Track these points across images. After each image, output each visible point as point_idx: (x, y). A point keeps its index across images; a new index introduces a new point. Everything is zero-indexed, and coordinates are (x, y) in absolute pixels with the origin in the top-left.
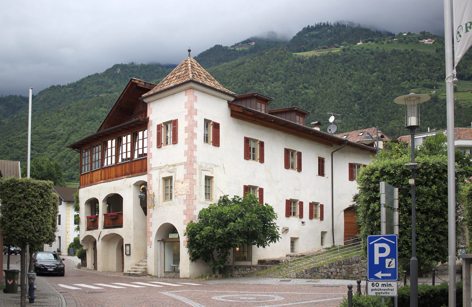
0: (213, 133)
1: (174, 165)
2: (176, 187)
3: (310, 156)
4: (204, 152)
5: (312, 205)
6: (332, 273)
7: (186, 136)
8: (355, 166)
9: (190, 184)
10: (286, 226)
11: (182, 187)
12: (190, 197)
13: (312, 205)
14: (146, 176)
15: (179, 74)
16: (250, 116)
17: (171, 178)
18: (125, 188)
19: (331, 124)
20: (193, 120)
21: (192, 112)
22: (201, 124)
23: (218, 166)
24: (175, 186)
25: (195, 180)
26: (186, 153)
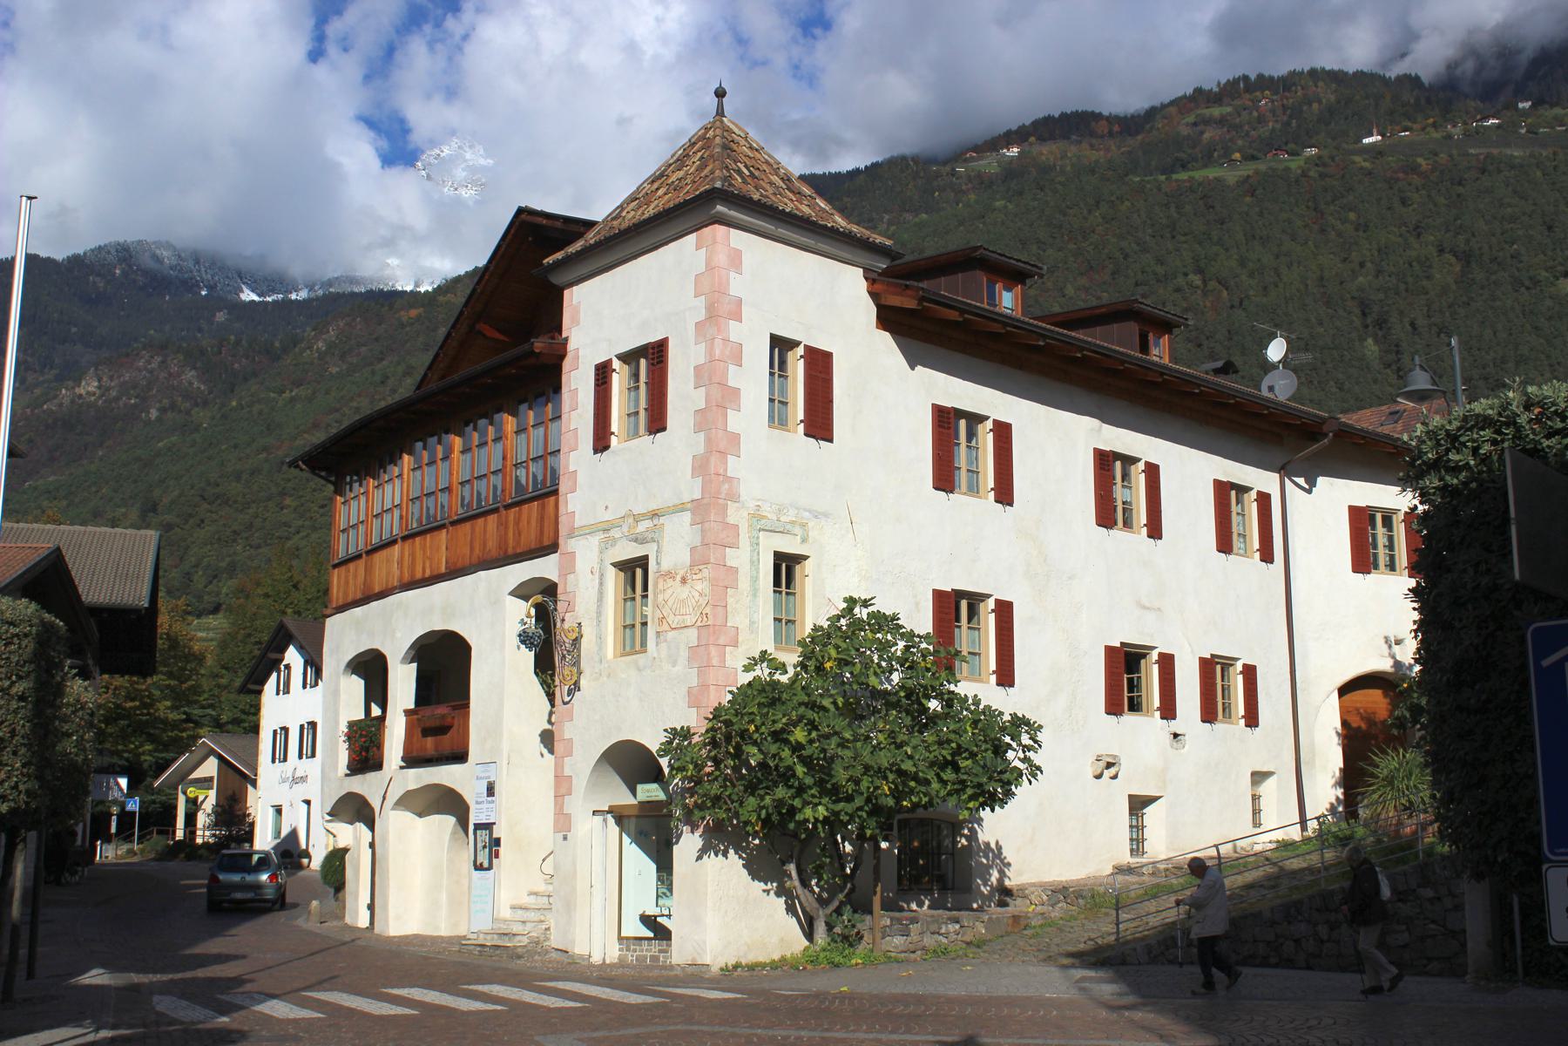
0: (813, 393)
1: (654, 515)
2: (660, 597)
3: (1189, 472)
4: (771, 461)
5: (1211, 668)
6: (1297, 941)
7: (699, 399)
8: (1372, 519)
9: (714, 583)
10: (1108, 749)
11: (684, 596)
12: (713, 631)
13: (1211, 668)
14: (553, 559)
15: (681, 174)
16: (954, 324)
17: (643, 562)
18: (485, 611)
19: (1274, 366)
20: (726, 340)
21: (720, 311)
22: (759, 354)
23: (826, 515)
24: (655, 595)
25: (734, 571)
26: (700, 466)
